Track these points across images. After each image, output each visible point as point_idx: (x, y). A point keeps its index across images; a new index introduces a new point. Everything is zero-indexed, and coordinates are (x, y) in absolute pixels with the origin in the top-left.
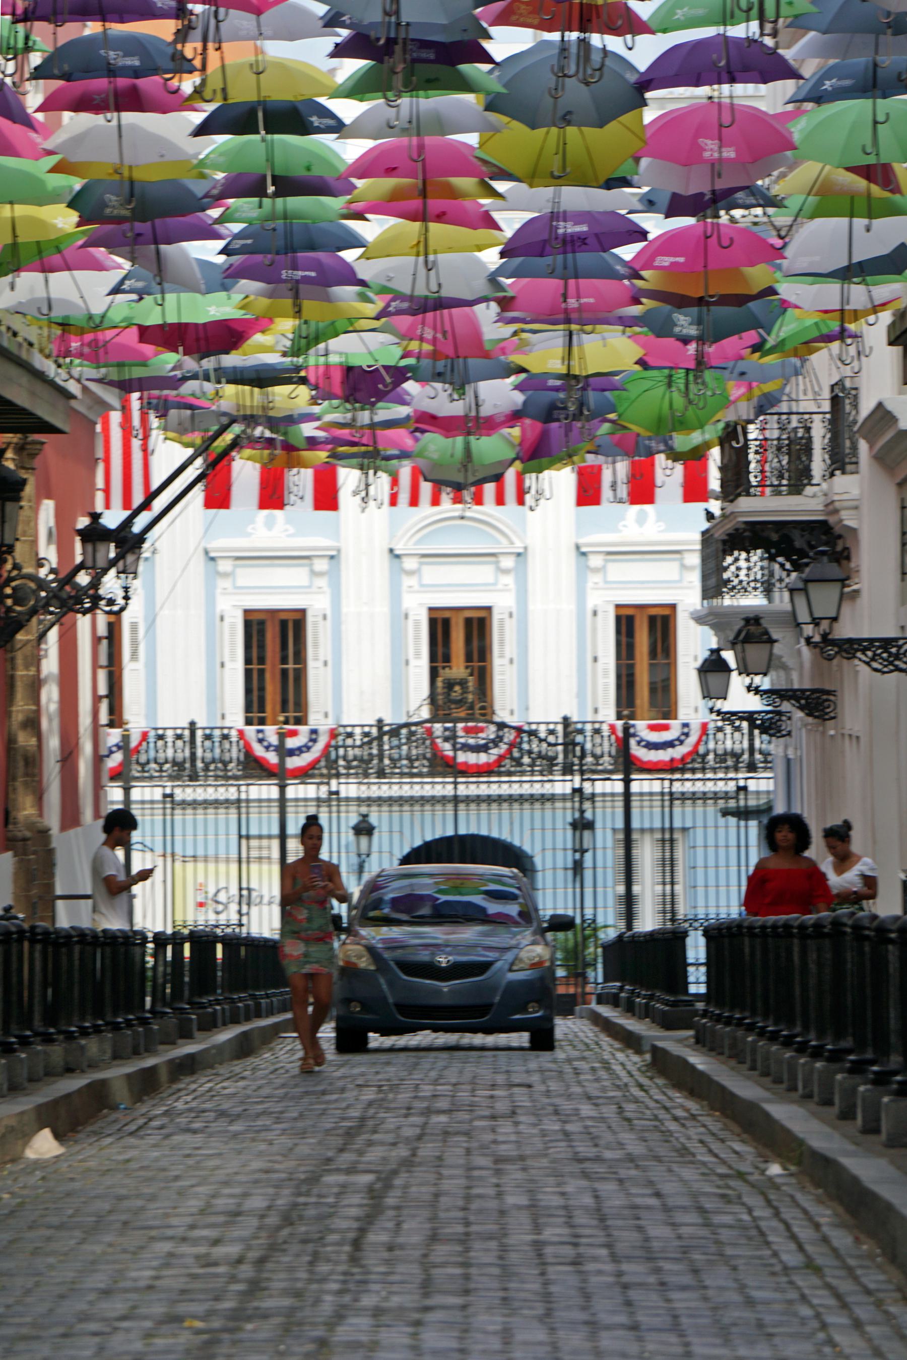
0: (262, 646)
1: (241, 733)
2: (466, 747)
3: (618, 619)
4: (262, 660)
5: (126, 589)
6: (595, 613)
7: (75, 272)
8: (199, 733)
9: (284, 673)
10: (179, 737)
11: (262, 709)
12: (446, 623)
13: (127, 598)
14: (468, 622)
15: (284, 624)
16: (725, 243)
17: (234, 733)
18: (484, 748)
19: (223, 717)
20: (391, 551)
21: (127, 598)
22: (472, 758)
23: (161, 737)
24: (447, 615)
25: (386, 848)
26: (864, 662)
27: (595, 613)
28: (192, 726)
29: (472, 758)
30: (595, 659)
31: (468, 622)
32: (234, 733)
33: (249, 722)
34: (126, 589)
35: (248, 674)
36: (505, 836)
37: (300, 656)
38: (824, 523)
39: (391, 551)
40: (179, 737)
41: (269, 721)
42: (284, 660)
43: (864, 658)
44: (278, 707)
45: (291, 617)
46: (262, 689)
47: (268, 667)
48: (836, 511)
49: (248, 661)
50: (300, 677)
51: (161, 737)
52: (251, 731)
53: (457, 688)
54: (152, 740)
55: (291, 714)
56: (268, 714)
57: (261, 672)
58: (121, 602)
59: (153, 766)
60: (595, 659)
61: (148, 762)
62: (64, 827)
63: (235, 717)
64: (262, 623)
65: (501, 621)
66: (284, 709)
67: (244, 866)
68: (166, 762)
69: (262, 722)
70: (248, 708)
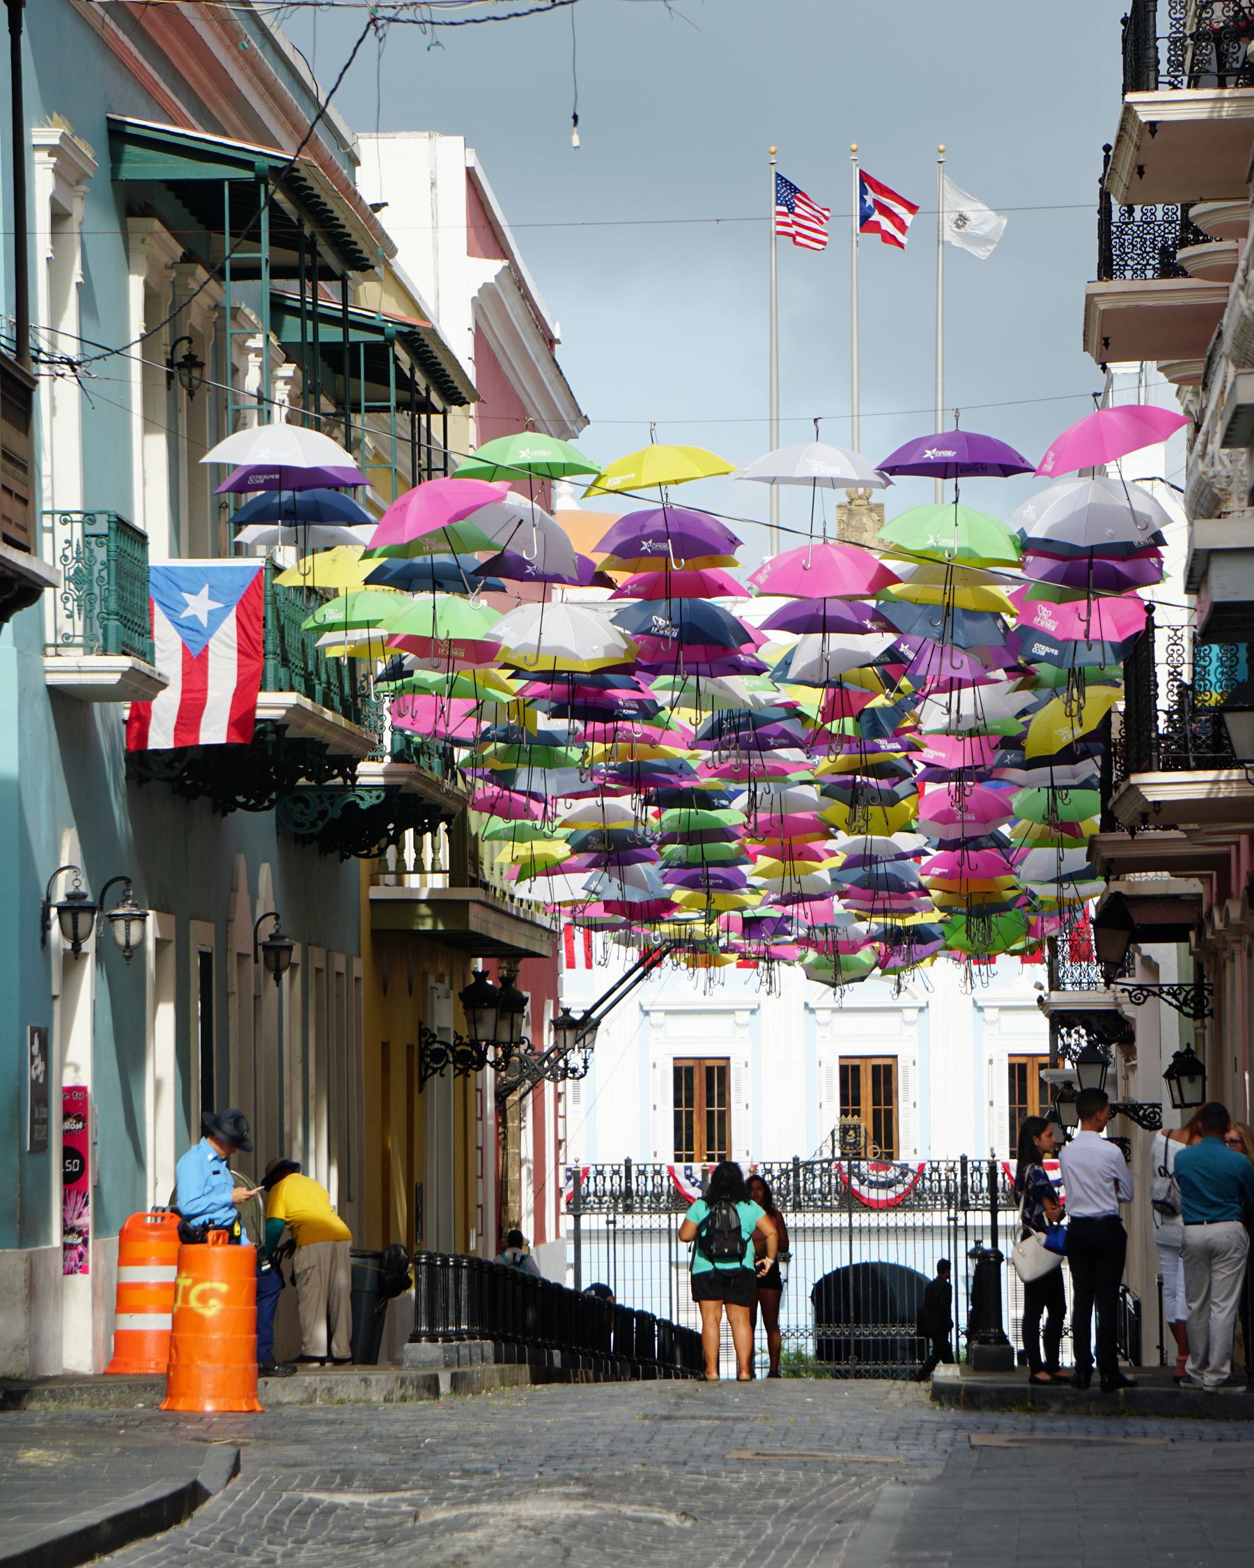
0: (690, 1089)
1: (671, 1171)
2: (873, 1185)
3: (1011, 1067)
4: (690, 1102)
5: (586, 1061)
6: (991, 1062)
7: (567, 876)
8: (634, 1169)
9: (710, 1114)
10: (616, 1173)
11: (690, 1147)
12: (856, 1069)
13: (586, 1068)
14: (876, 1069)
15: (710, 1070)
16: (973, 867)
17: (664, 1169)
18: (888, 1185)
19: (655, 1154)
20: (806, 1005)
21: (586, 1068)
22: (874, 1194)
23: (600, 1173)
24: (857, 1062)
25: (801, 1273)
26: (1175, 1007)
27: (991, 1062)
28: (964, 1160)
29: (874, 1194)
30: (991, 1104)
31: (876, 1069)
32: (664, 1169)
33: (678, 1159)
34: (586, 1061)
35: (677, 1116)
36: (910, 1264)
37: (724, 1099)
38: (1115, 1012)
39: (806, 1005)
40: (616, 1173)
41: (696, 1158)
42: (710, 1103)
43: (1175, 1002)
44: (705, 1146)
45: (716, 1063)
46: (690, 1127)
47: (695, 1109)
48: (1120, 1005)
49: (677, 1103)
50: (724, 1117)
51: (600, 1173)
52: (680, 1167)
53: (851, 1132)
54: (592, 1175)
55: (850, 1108)
56: (696, 1152)
57: (689, 1115)
58: (582, 1070)
59: (592, 1198)
60: (991, 1104)
61: (588, 1195)
62: (535, 1244)
63: (666, 1154)
64: (690, 1071)
65: (906, 1068)
66: (710, 1147)
67: (674, 1270)
68: (605, 1195)
69: (690, 1159)
70: (678, 1147)
